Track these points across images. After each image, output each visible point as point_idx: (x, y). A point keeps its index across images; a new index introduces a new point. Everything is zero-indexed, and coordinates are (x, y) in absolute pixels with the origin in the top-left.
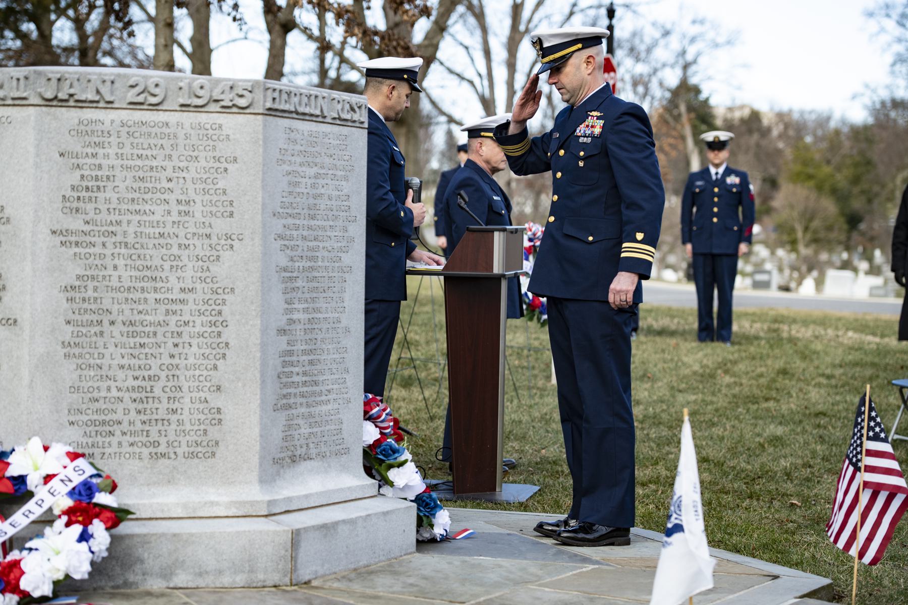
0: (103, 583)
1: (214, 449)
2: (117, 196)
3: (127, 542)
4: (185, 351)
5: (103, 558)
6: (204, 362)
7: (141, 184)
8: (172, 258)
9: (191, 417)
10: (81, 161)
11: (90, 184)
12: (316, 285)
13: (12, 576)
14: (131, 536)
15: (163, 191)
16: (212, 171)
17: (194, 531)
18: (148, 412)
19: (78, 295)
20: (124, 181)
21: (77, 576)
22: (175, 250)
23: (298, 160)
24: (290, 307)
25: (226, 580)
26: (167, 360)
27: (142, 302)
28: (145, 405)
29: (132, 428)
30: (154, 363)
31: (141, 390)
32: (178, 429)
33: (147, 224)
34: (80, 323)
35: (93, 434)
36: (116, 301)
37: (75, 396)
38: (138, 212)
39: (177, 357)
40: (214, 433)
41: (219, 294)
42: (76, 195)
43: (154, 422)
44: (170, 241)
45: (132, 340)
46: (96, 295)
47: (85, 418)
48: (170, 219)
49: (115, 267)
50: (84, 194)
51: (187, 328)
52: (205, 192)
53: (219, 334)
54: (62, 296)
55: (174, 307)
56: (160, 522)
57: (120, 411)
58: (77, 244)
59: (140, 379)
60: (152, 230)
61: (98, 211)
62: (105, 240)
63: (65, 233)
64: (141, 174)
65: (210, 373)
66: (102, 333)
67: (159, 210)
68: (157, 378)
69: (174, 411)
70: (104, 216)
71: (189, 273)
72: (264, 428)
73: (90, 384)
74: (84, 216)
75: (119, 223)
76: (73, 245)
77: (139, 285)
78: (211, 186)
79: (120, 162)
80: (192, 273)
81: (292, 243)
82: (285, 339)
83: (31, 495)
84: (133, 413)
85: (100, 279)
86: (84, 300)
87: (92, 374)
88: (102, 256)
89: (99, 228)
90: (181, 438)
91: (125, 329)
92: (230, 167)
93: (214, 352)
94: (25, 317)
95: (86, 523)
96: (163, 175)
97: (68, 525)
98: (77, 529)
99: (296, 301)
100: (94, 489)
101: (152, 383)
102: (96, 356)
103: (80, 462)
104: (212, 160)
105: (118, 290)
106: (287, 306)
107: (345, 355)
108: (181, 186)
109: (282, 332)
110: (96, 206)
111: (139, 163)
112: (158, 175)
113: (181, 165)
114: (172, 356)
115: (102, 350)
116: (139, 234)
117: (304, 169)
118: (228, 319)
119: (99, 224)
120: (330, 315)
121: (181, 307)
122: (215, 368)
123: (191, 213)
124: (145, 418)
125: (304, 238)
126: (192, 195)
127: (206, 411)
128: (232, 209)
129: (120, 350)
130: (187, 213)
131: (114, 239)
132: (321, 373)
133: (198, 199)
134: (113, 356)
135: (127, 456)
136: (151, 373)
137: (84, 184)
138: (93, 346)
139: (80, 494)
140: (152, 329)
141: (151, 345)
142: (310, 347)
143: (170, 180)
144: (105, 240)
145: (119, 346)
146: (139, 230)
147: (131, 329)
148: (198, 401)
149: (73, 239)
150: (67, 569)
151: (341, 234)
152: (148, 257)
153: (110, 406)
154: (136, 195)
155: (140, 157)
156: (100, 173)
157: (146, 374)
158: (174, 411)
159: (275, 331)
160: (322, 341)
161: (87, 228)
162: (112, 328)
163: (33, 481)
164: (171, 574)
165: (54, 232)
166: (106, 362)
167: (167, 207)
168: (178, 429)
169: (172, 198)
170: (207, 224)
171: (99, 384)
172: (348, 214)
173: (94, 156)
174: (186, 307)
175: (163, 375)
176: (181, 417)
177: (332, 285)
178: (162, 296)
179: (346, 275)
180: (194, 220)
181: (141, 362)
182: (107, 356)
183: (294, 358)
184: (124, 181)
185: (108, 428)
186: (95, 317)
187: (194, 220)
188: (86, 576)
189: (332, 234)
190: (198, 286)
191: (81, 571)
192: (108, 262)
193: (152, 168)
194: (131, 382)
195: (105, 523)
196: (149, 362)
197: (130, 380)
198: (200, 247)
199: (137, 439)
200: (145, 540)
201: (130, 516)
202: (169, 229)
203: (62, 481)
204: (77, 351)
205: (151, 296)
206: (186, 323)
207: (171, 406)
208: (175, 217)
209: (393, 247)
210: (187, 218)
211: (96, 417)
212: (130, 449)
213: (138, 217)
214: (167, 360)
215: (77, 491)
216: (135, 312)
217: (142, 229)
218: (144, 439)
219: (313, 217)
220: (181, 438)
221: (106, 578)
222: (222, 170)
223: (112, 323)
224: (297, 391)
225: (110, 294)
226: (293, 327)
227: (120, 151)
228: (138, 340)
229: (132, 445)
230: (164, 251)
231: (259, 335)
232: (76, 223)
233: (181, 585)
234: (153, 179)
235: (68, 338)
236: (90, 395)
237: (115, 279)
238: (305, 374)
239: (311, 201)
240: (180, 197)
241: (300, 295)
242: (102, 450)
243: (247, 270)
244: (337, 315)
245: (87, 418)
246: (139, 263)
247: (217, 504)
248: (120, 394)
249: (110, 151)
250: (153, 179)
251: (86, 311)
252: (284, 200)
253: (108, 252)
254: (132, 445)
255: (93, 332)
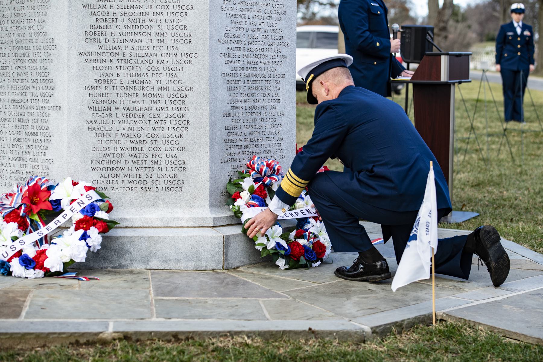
0: (106, 265)
1: (181, 186)
2: (119, 31)
3: (120, 241)
4: (162, 126)
5: (98, 250)
6: (174, 132)
7: (133, 23)
8: (153, 69)
9: (166, 166)
10: (96, 10)
11: (102, 24)
12: (255, 85)
13: (41, 259)
14: (117, 238)
15: (147, 27)
16: (177, 14)
17: (161, 235)
18: (140, 163)
19: (96, 92)
20: (123, 22)
21: (77, 260)
22: (155, 64)
23: (239, 7)
24: (233, 98)
25: (182, 266)
26: (151, 131)
27: (135, 96)
28: (138, 159)
29: (130, 172)
30: (143, 133)
31: (135, 149)
32: (159, 173)
33: (137, 48)
34: (97, 109)
35: (107, 176)
36: (119, 95)
37: (95, 152)
38: (131, 41)
39: (157, 129)
40: (181, 176)
41: (183, 91)
42: (93, 30)
43: (143, 169)
44: (151, 58)
45: (129, 119)
46: (107, 91)
47: (101, 166)
48: (151, 45)
49: (118, 75)
50: (98, 30)
51: (163, 111)
52: (174, 28)
53: (183, 115)
54: (87, 92)
55: (155, 99)
56: (146, 229)
57: (123, 162)
58: (95, 60)
59: (135, 143)
60: (140, 52)
61: (107, 41)
62: (112, 58)
63: (87, 54)
64: (133, 17)
65: (178, 139)
66: (111, 115)
67: (145, 39)
68: (145, 142)
69: (156, 163)
70: (111, 43)
71: (164, 78)
72: (213, 173)
73: (104, 145)
74: (98, 44)
75: (120, 48)
76: (92, 61)
77: (133, 85)
78: (177, 24)
79: (120, 10)
80: (166, 78)
81: (235, 59)
82: (229, 119)
83: (62, 210)
84: (131, 163)
85: (109, 82)
86: (99, 94)
87: (105, 139)
88: (110, 68)
89: (108, 51)
90: (160, 179)
91: (125, 112)
92: (189, 12)
93: (180, 126)
94: (65, 106)
95: (86, 229)
96: (147, 18)
97: (76, 229)
98: (81, 232)
99: (239, 95)
100: (96, 209)
101: (142, 145)
102: (107, 129)
103: (91, 192)
104: (178, 8)
105: (120, 88)
106: (231, 98)
107: (280, 129)
108: (158, 24)
109: (227, 114)
110: (106, 37)
111: (132, 10)
112: (144, 18)
113: (158, 11)
114: (154, 129)
115: (111, 125)
116: (132, 54)
117: (244, 13)
118: (189, 106)
119: (108, 48)
120: (267, 104)
121: (159, 99)
122: (181, 136)
123: (165, 41)
124: (138, 166)
125: (245, 56)
126: (165, 30)
127: (176, 163)
128: (190, 38)
129: (122, 125)
130: (162, 41)
131: (117, 57)
132: (260, 139)
133: (169, 32)
134: (118, 129)
135: (128, 189)
136: (142, 139)
137: (98, 24)
138: (106, 122)
139: (87, 211)
140: (141, 112)
141: (141, 122)
142: (251, 124)
143: (151, 21)
144: (112, 58)
145: (122, 122)
146: (132, 51)
147: (128, 112)
148: (171, 156)
149: (92, 58)
150: (71, 256)
151: (276, 54)
152: (138, 68)
153: (116, 159)
154: (130, 30)
155: (132, 7)
156: (108, 17)
157: (138, 140)
158: (156, 163)
159: (222, 114)
160: (261, 120)
161: (101, 51)
162: (117, 112)
163: (64, 204)
164: (148, 260)
165: (81, 54)
166: (113, 132)
167: (149, 37)
168: (159, 173)
169: (153, 32)
170: (175, 48)
171: (110, 145)
172: (281, 41)
173: (105, 6)
174: (162, 99)
175: (149, 140)
176: (160, 166)
177: (269, 85)
178: (148, 92)
179: (280, 79)
180: (167, 45)
181: (135, 133)
182: (114, 129)
183: (238, 131)
184: (123, 22)
185: (115, 172)
186: (106, 105)
187: (167, 45)
188: (84, 261)
189: (268, 54)
190: (170, 86)
191: (81, 257)
192: (114, 71)
193: (140, 14)
194: (129, 145)
195: (98, 229)
196: (140, 132)
197: (129, 143)
198: (171, 62)
199: (133, 179)
200: (132, 240)
201: (116, 226)
202: (151, 51)
203: (78, 203)
204: (95, 125)
205: (141, 93)
206: (163, 109)
207: (154, 159)
208: (154, 43)
209: (374, 65)
210: (162, 44)
211: (108, 165)
212: (129, 185)
213: (132, 44)
214: (151, 131)
215: (85, 210)
216: (131, 102)
217: (134, 51)
218: (138, 179)
219: (252, 43)
220: (160, 179)
221: (108, 262)
222: (184, 14)
223: (117, 109)
224: (241, 151)
225: (115, 91)
226: (236, 111)
227: (120, 4)
228: (133, 119)
229: (130, 182)
230: (148, 64)
231: (208, 116)
232: (94, 48)
233: (155, 268)
234: (141, 20)
235: (90, 118)
236: (104, 152)
237: (118, 82)
238: (246, 140)
239: (250, 33)
240: (158, 31)
241: (242, 91)
242: (113, 186)
243: (200, 76)
244: (273, 104)
245: (103, 166)
246: (132, 72)
247: (182, 219)
248: (122, 152)
249: (114, 3)
250: (141, 20)
251: (101, 101)
252: (228, 32)
253: (114, 65)
254: (130, 182)
255: (105, 114)
